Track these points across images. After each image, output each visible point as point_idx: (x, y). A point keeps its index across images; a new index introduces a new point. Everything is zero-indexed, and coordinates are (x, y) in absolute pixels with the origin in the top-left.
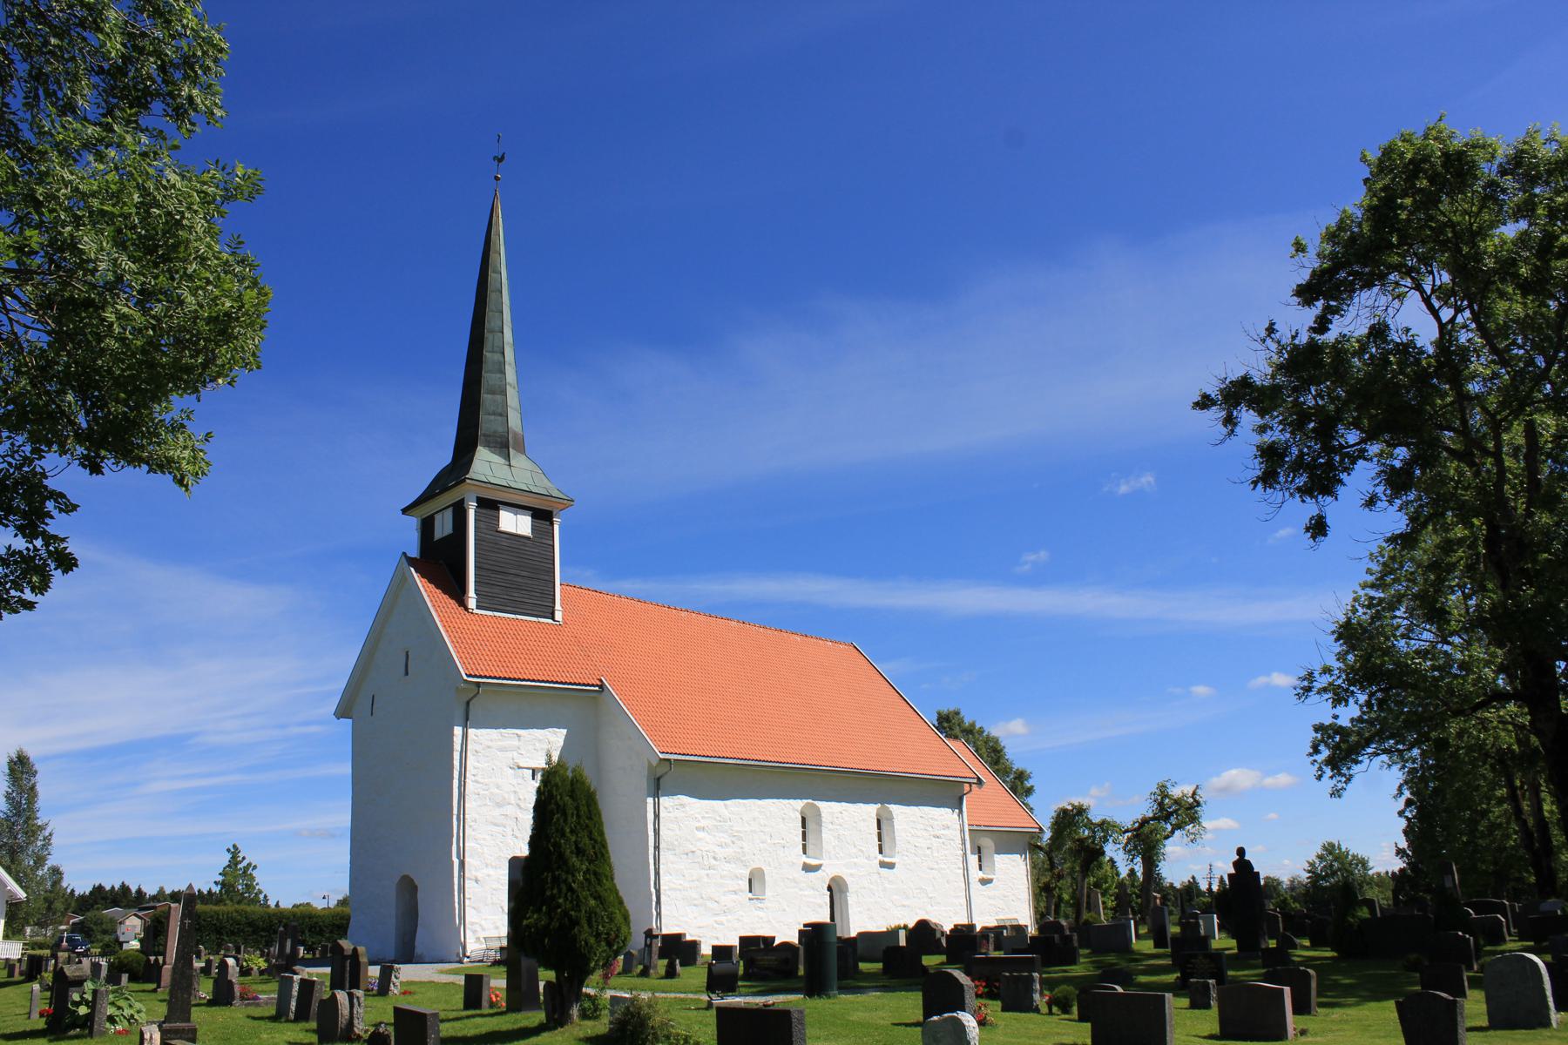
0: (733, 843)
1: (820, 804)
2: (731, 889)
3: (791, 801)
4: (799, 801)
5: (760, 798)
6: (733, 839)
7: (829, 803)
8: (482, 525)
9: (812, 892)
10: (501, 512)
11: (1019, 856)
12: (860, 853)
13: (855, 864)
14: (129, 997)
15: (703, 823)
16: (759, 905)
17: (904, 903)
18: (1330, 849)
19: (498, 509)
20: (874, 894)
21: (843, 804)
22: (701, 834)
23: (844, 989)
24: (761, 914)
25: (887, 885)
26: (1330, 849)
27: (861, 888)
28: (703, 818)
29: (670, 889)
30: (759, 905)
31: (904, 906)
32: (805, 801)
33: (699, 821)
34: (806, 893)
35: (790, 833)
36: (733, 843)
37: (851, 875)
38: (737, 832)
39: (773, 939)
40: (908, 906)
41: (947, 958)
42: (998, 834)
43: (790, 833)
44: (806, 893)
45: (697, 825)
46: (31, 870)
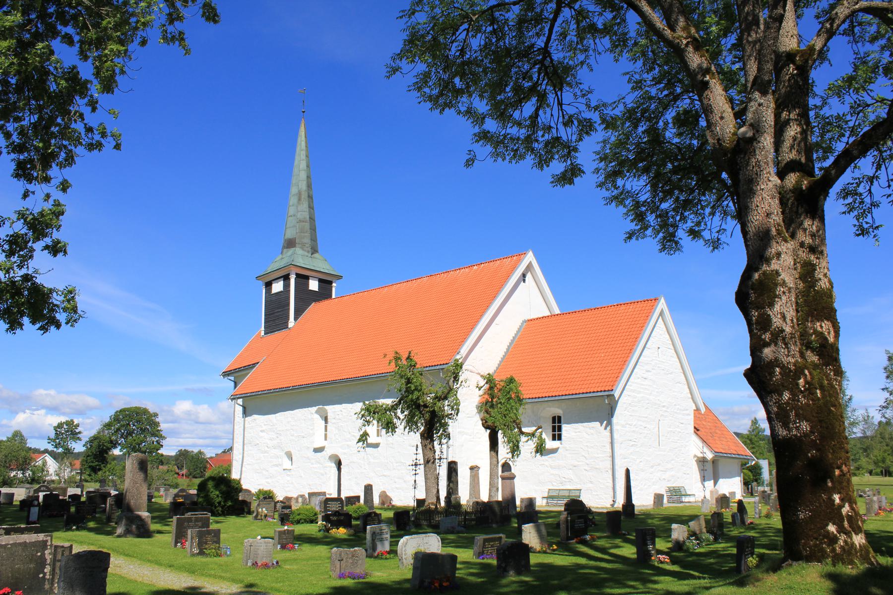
3: (310, 409)
7: (334, 406)
8: (267, 295)
9: (319, 465)
10: (310, 281)
11: (597, 424)
12: (353, 438)
13: (348, 445)
14: (267, 484)
15: (264, 428)
16: (289, 473)
17: (385, 474)
18: (655, 494)
19: (309, 279)
21: (343, 405)
22: (262, 434)
24: (289, 478)
26: (655, 494)
27: (351, 462)
29: (248, 464)
30: (289, 473)
31: (385, 476)
32: (317, 407)
33: (262, 427)
34: (315, 466)
37: (345, 454)
38: (280, 431)
39: (701, 461)
40: (389, 476)
42: (567, 401)
44: (315, 466)
45: (261, 429)
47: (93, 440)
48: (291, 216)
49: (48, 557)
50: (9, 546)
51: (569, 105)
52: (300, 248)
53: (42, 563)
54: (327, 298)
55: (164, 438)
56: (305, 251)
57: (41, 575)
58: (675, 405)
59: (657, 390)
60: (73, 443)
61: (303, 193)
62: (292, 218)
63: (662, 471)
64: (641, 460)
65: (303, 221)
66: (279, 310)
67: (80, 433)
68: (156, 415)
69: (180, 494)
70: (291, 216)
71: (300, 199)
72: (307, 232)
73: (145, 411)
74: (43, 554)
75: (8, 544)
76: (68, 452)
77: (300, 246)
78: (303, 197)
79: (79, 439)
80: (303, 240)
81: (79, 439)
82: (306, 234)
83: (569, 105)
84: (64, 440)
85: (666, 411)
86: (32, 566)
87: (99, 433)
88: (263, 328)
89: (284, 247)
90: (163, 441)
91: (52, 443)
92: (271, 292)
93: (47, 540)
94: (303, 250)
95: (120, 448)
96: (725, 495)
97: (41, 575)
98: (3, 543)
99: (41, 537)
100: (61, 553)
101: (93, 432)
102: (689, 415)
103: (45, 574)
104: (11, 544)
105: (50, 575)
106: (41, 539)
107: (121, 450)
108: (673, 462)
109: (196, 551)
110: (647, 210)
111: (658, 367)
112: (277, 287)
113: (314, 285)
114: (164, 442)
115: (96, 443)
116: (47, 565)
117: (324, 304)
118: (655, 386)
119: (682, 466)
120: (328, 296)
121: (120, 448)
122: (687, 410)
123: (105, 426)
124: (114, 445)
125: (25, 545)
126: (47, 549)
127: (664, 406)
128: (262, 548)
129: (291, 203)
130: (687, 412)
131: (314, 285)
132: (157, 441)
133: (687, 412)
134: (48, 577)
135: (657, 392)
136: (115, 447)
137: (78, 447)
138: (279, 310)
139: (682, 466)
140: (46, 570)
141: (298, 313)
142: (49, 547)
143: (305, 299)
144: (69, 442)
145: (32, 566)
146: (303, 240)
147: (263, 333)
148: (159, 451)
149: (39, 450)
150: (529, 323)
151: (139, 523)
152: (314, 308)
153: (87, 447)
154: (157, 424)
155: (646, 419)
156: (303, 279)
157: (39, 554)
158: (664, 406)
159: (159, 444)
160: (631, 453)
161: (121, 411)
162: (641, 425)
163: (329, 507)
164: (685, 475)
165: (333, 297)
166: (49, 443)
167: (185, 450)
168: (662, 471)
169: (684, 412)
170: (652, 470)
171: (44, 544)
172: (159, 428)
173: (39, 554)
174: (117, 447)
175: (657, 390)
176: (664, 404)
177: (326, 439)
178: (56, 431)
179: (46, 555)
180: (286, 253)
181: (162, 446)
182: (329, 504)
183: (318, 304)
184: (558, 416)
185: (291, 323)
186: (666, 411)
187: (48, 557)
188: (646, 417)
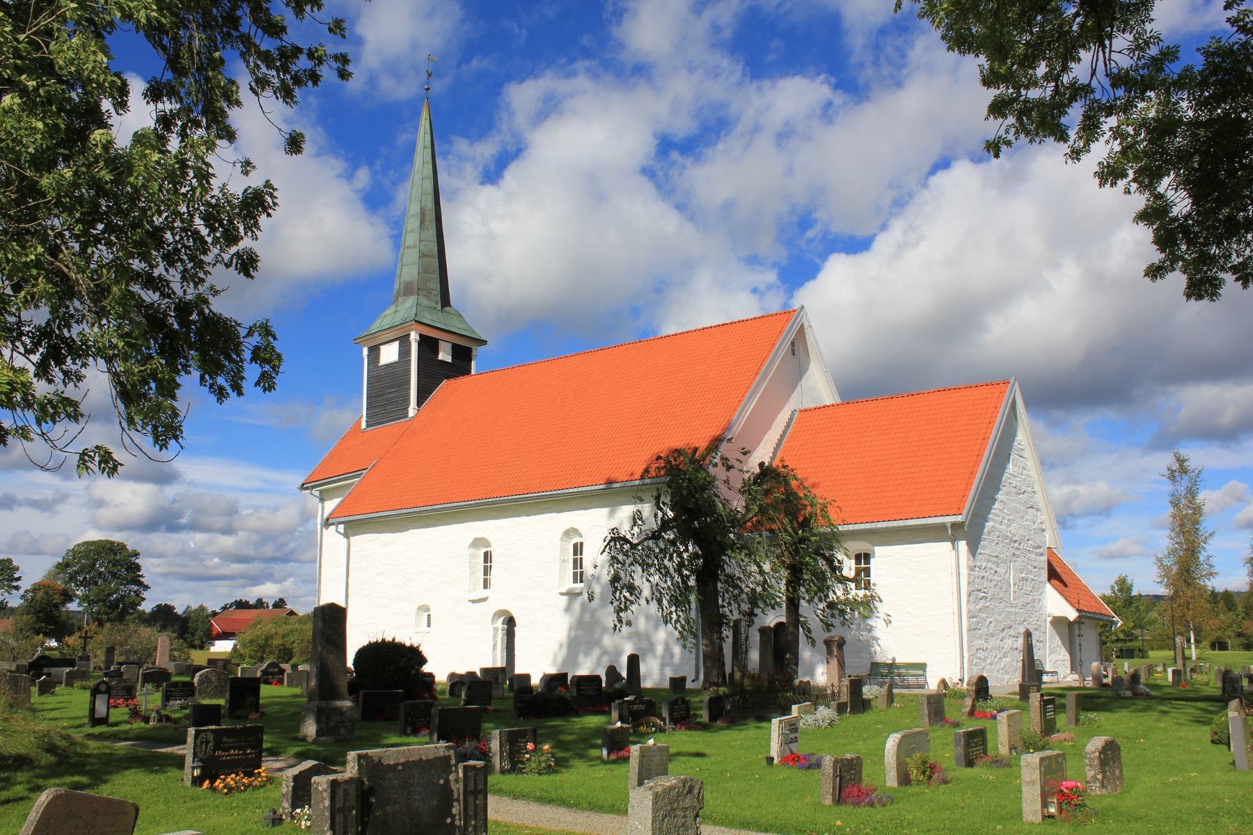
8: (372, 366)
47: (36, 588)
49: (457, 788)
50: (400, 768)
51: (1120, 52)
53: (446, 797)
54: (463, 375)
55: (146, 587)
56: (431, 300)
57: (449, 821)
58: (1028, 540)
59: (1008, 517)
61: (428, 213)
62: (410, 250)
63: (1014, 636)
64: (991, 620)
65: (428, 256)
66: (392, 390)
67: (19, 579)
68: (136, 554)
69: (270, 670)
70: (410, 247)
71: (422, 222)
73: (122, 547)
74: (447, 782)
75: (398, 764)
77: (424, 293)
81: (17, 588)
83: (1120, 52)
85: (1018, 549)
86: (435, 803)
88: (364, 418)
90: (145, 593)
92: (379, 362)
93: (450, 756)
97: (449, 821)
98: (392, 762)
100: (473, 780)
102: (1041, 555)
103: (453, 817)
104: (402, 764)
105: (460, 819)
106: (442, 754)
109: (507, 766)
111: (1010, 483)
112: (389, 354)
113: (445, 355)
114: (145, 594)
115: (41, 594)
116: (454, 800)
117: (462, 381)
118: (1005, 511)
120: (467, 371)
121: (78, 601)
122: (1040, 547)
123: (57, 567)
124: (68, 597)
126: (452, 772)
127: (1015, 542)
129: (409, 227)
130: (1041, 551)
131: (445, 355)
132: (135, 592)
133: (1041, 551)
134: (457, 823)
135: (1009, 520)
137: (14, 601)
138: (392, 390)
140: (454, 811)
141: (422, 397)
142: (453, 769)
143: (432, 375)
147: (364, 425)
149: (247, 602)
150: (805, 414)
151: (338, 719)
152: (446, 387)
155: (996, 560)
156: (428, 346)
158: (1015, 542)
159: (138, 595)
162: (991, 569)
163: (582, 690)
165: (473, 372)
167: (166, 604)
168: (1014, 636)
170: (1003, 635)
172: (140, 573)
173: (442, 781)
174: (72, 601)
175: (1008, 517)
177: (485, 587)
179: (452, 783)
181: (144, 599)
183: (452, 381)
185: (412, 412)
186: (1018, 549)
187: (457, 788)
188: (997, 557)
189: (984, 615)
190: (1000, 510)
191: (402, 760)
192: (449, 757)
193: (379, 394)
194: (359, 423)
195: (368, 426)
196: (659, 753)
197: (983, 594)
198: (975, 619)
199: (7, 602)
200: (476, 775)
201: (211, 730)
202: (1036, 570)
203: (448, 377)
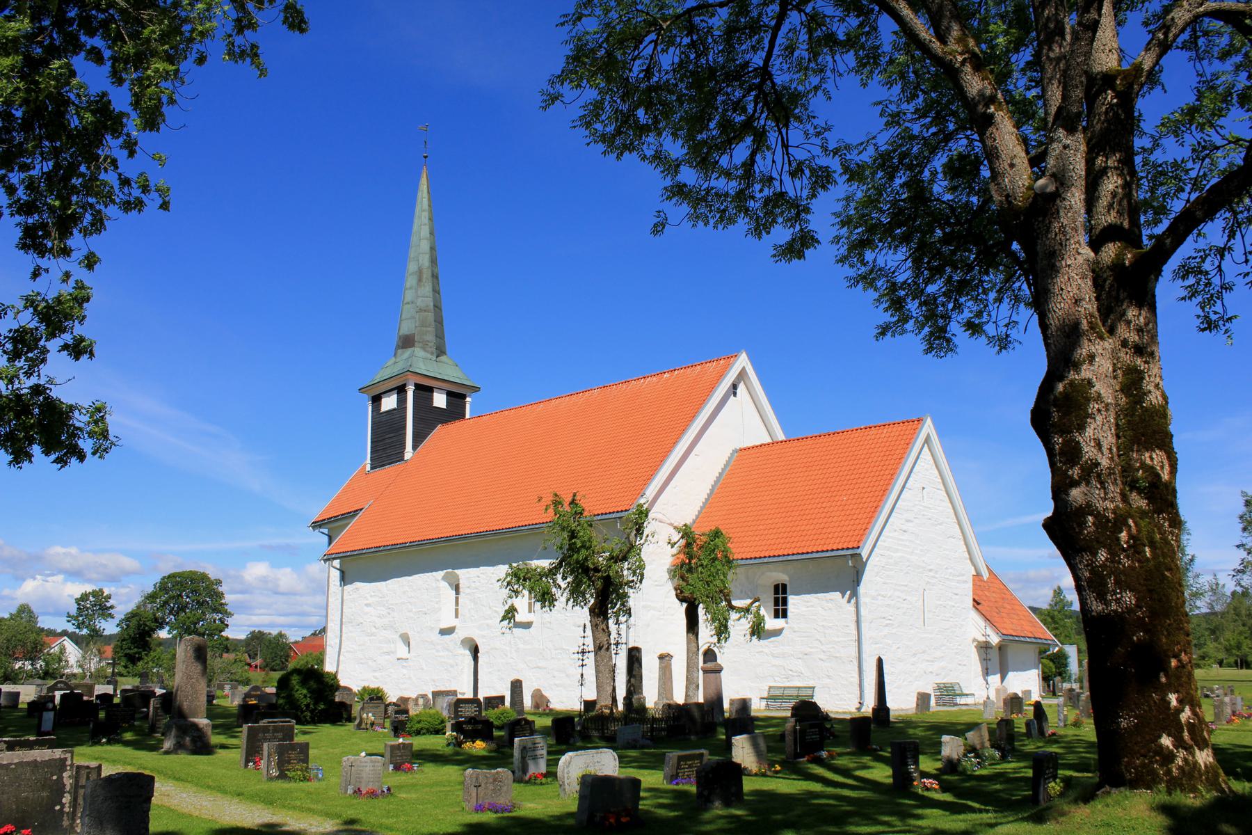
0: (389, 614)
1: (458, 572)
2: (385, 650)
3: (434, 573)
4: (440, 572)
5: (410, 574)
6: (389, 611)
7: (469, 570)
8: (375, 414)
10: (435, 394)
11: (838, 594)
13: (488, 625)
15: (370, 600)
16: (405, 664)
18: (919, 693)
19: (433, 392)
20: (506, 656)
21: (481, 568)
22: (367, 609)
23: (1246, 669)
24: (405, 671)
25: (521, 646)
26: (919, 693)
27: (492, 649)
28: (371, 596)
29: (347, 652)
30: (405, 664)
31: (538, 667)
34: (441, 654)
35: (431, 601)
36: (389, 614)
37: (483, 637)
38: (392, 604)
40: (545, 668)
41: (1161, 671)
42: (795, 563)
43: (431, 601)
44: (441, 654)
45: (366, 602)
46: (1112, 562)
47: (131, 616)
48: (408, 303)
49: (68, 782)
50: (13, 766)
51: (798, 147)
52: (421, 347)
53: (59, 789)
54: (459, 419)
55: (230, 615)
56: (428, 352)
57: (58, 808)
58: (946, 568)
60: (103, 621)
61: (425, 271)
62: (409, 306)
63: (928, 661)
64: (898, 646)
65: (425, 311)
66: (392, 435)
67: (112, 607)
68: (219, 582)
71: (420, 280)
72: (430, 325)
73: (204, 577)
74: (60, 778)
75: (11, 764)
76: (96, 634)
77: (421, 345)
78: (425, 276)
79: (111, 616)
80: (425, 337)
81: (111, 616)
82: (429, 329)
83: (798, 147)
84: (90, 617)
85: (934, 577)
86: (44, 794)
87: (138, 607)
89: (398, 347)
90: (229, 619)
91: (73, 622)
92: (380, 410)
94: (425, 351)
95: (168, 628)
96: (1016, 694)
97: (58, 808)
98: (5, 763)
99: (58, 753)
101: (131, 607)
102: (965, 582)
103: (63, 805)
104: (15, 764)
105: (70, 807)
106: (58, 757)
107: (169, 632)
108: (943, 648)
109: (274, 773)
110: (907, 295)
112: (389, 403)
113: (440, 400)
114: (229, 621)
115: (134, 622)
116: (65, 792)
117: (455, 426)
119: (956, 653)
120: (460, 415)
121: (168, 628)
122: (963, 575)
124: (160, 624)
125: (34, 764)
127: (931, 570)
128: (368, 769)
129: (408, 285)
130: (964, 578)
131: (440, 400)
132: (220, 619)
134: (67, 809)
135: (921, 550)
136: (162, 628)
137: (110, 627)
138: (392, 435)
139: (956, 653)
140: (64, 800)
141: (418, 439)
142: (68, 768)
143: (428, 419)
144: (97, 621)
145: (44, 794)
146: (425, 337)
147: (368, 467)
148: (223, 633)
149: (55, 631)
151: (195, 734)
152: (440, 432)
153: (122, 628)
154: (220, 595)
156: (424, 391)
157: (55, 777)
158: (931, 570)
159: (223, 622)
160: (885, 636)
161: (169, 577)
162: (899, 597)
163: (461, 711)
164: (960, 667)
165: (468, 416)
166: (68, 621)
167: (259, 632)
168: (928, 661)
169: (960, 578)
170: (914, 659)
171: (61, 765)
172: (223, 601)
173: (55, 777)
174: (163, 628)
176: (930, 567)
177: (457, 616)
178: (79, 604)
179: (65, 779)
180: (401, 355)
181: (227, 626)
182: (461, 707)
183: (445, 426)
184: (782, 584)
185: (409, 453)
186: (934, 577)
187: (68, 782)
188: (906, 586)
189: (890, 642)
190: (910, 541)
191: (16, 761)
192: (66, 759)
193: (380, 439)
194: (365, 466)
195: (372, 468)
196: (371, 764)
197: (888, 622)
198: (877, 646)
199: (104, 629)
200: (88, 774)
201: (5, 742)
202: (957, 597)
203: (442, 423)
